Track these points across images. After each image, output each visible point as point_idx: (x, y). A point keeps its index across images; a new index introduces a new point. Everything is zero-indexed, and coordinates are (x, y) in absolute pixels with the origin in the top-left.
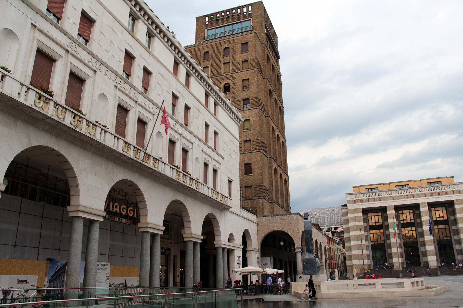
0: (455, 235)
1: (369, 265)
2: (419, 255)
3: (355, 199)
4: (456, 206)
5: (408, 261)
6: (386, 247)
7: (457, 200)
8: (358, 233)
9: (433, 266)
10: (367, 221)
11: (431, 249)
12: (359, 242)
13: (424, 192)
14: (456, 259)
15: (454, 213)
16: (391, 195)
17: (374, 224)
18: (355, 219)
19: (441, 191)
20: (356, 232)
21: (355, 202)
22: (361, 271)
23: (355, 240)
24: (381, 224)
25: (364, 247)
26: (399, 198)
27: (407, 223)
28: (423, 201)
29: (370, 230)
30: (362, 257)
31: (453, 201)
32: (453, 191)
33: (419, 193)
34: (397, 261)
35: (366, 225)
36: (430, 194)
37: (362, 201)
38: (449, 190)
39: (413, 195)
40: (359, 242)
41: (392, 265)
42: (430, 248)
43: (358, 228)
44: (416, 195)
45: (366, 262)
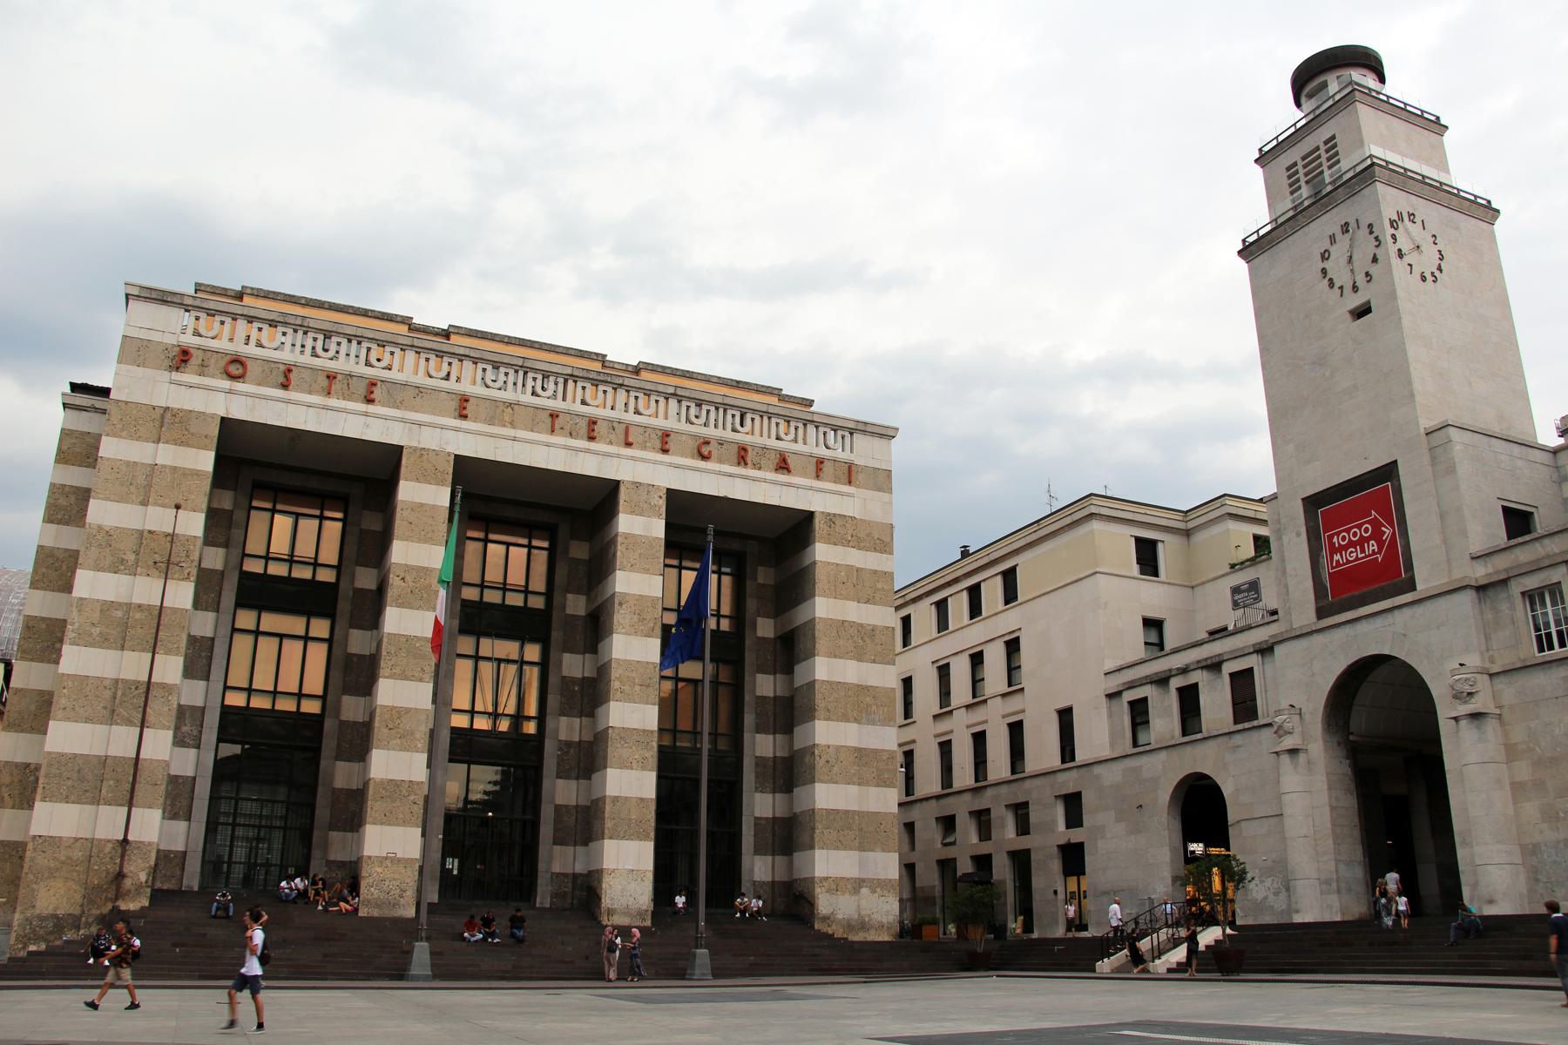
0: (766, 732)
1: (167, 861)
2: (535, 824)
3: (189, 340)
4: (823, 552)
5: (453, 864)
6: (329, 745)
7: (831, 518)
8: (145, 590)
9: (627, 912)
10: (237, 533)
11: (634, 793)
12: (131, 665)
13: (660, 423)
14: (745, 877)
15: (794, 586)
16: (451, 385)
17: (277, 569)
18: (144, 485)
19: (756, 440)
20: (125, 579)
21: (182, 358)
22: (91, 894)
23: (104, 642)
24: (326, 576)
25: (161, 710)
26: (503, 413)
27: (502, 607)
28: (647, 475)
29: (240, 604)
30: (126, 782)
31: (809, 516)
32: (820, 462)
33: (631, 417)
34: (393, 851)
35: (215, 558)
36: (693, 444)
37: (236, 368)
38: (799, 447)
39: (593, 422)
40: (131, 665)
41: (585, 892)
42: (631, 783)
43: (161, 556)
44: (612, 424)
45: (150, 826)
